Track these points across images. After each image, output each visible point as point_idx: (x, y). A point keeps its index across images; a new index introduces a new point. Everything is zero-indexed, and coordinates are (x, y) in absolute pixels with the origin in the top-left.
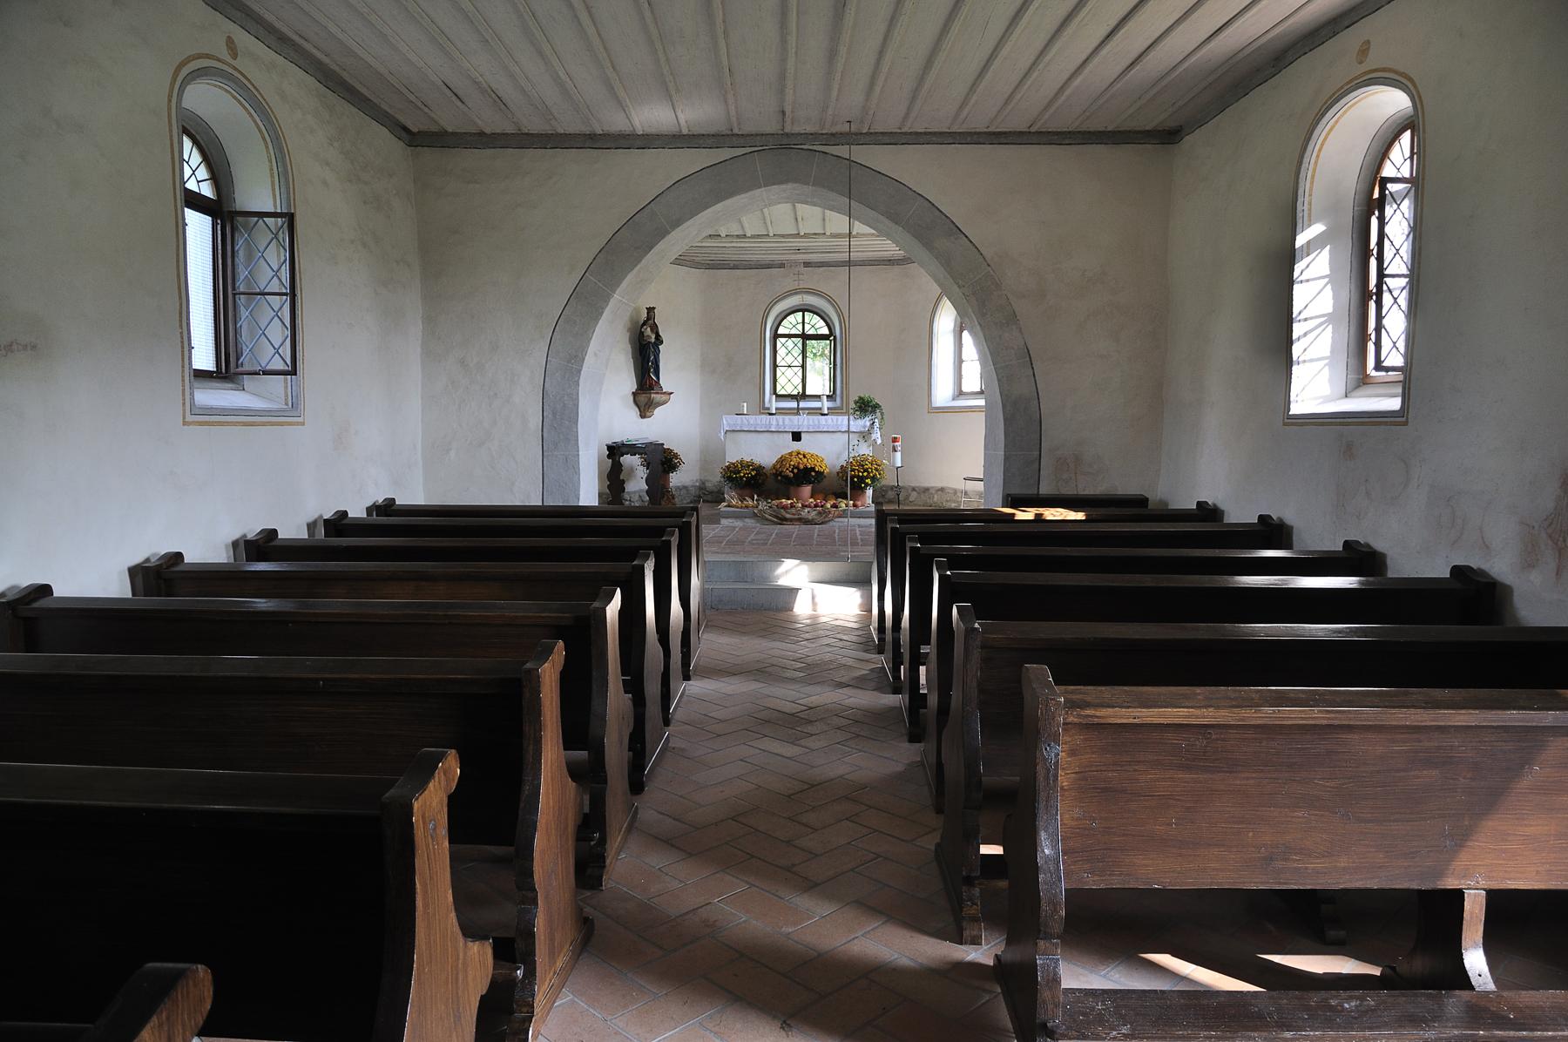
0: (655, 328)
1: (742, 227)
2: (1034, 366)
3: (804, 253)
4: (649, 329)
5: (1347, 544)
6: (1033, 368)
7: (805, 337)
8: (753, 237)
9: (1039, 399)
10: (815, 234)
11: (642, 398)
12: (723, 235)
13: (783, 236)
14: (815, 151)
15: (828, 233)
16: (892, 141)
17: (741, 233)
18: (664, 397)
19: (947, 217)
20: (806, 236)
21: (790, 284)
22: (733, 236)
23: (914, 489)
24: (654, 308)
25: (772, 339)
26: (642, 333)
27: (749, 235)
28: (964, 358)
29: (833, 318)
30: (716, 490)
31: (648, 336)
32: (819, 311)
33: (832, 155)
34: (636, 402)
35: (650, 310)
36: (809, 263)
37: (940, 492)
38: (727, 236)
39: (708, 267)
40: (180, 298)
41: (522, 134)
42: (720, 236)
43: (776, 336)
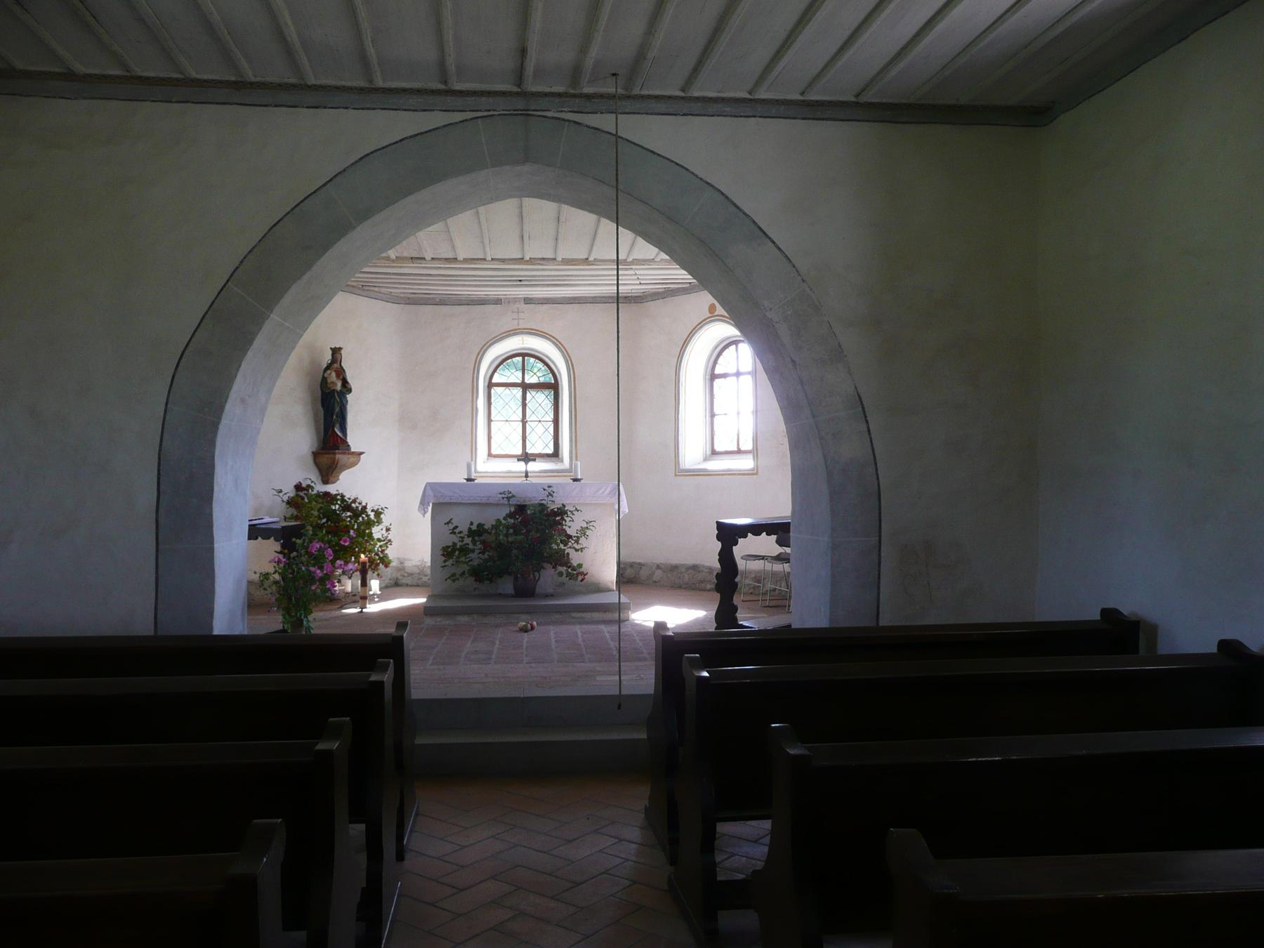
0: (341, 373)
1: (453, 247)
2: (868, 418)
3: (526, 286)
4: (334, 374)
5: (1105, 612)
6: (867, 422)
7: (525, 387)
8: (466, 261)
9: (876, 464)
10: (543, 259)
11: (325, 459)
12: (428, 258)
13: (503, 261)
14: (563, 120)
15: (559, 259)
16: (671, 111)
17: (451, 256)
18: (352, 459)
19: (744, 213)
20: (532, 261)
21: (507, 323)
22: (440, 259)
23: (658, 567)
24: (340, 349)
25: (486, 389)
26: (324, 380)
27: (460, 258)
28: (716, 410)
29: (558, 363)
30: (418, 571)
31: (332, 383)
32: (537, 354)
33: (589, 127)
34: (317, 464)
35: (336, 352)
36: (531, 299)
37: (690, 571)
38: (433, 259)
39: (408, 302)
40: (472, 454)
41: (132, 77)
42: (424, 259)
43: (490, 385)
